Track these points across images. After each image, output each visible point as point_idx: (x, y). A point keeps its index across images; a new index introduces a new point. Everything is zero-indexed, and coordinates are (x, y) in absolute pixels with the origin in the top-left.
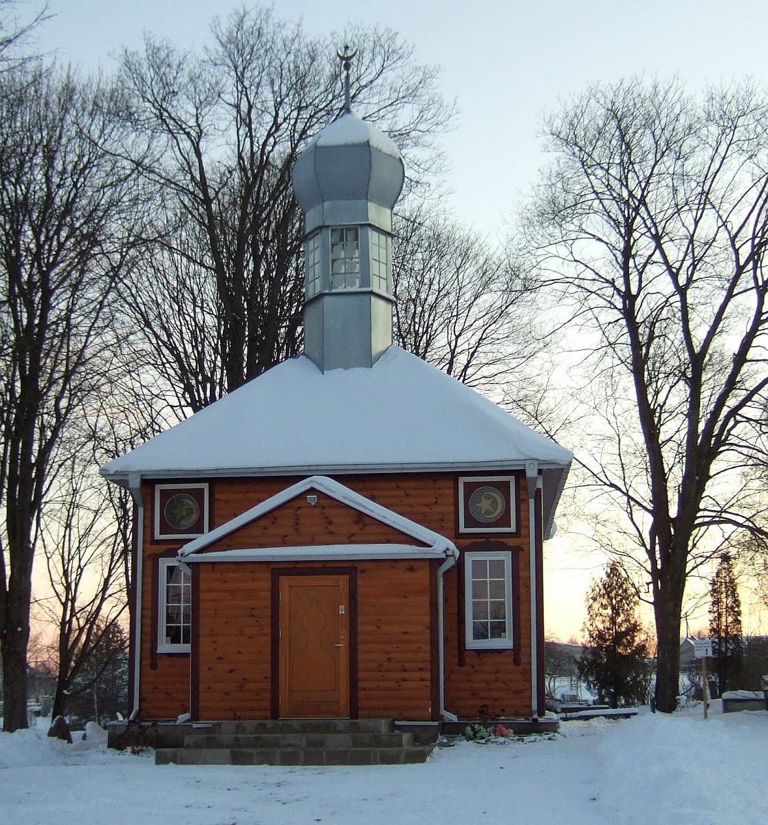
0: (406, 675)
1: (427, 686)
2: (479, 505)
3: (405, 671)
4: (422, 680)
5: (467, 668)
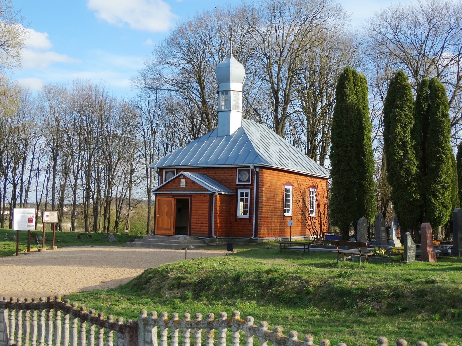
0: (202, 225)
5: (237, 223)
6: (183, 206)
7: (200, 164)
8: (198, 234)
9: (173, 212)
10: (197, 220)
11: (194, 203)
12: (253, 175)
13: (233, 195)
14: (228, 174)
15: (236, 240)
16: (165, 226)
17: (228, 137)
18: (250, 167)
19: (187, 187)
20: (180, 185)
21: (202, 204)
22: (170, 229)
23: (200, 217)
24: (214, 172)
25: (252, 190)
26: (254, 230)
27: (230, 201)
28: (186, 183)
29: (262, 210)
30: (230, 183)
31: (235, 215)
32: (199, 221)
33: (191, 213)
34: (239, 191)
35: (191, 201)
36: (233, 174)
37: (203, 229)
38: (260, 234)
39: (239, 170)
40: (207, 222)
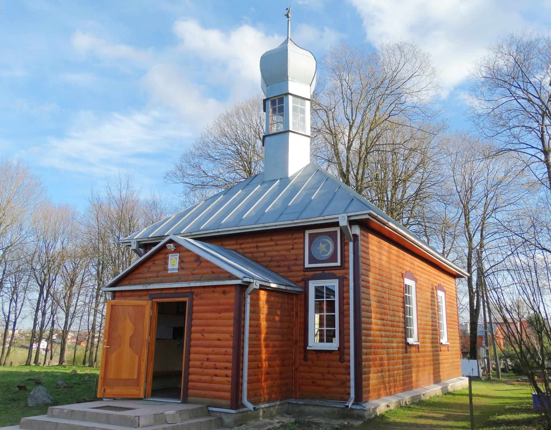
0: (217, 372)
1: (229, 381)
2: (318, 248)
3: (216, 368)
4: (227, 376)
5: (309, 363)
6: (172, 315)
7: (227, 225)
8: (205, 396)
9: (147, 337)
10: (205, 357)
11: (198, 312)
12: (344, 244)
13: (297, 294)
14: (283, 247)
15: (307, 409)
16: (125, 375)
17: (285, 180)
18: (336, 224)
19: (183, 272)
20: (166, 269)
21: (216, 315)
22: (137, 383)
23: (210, 350)
24: (254, 245)
25: (343, 281)
26: (352, 383)
27: (290, 305)
28: (181, 261)
29: (370, 329)
30: (289, 267)
31: (303, 344)
32: (208, 360)
33: (190, 339)
34: (312, 285)
35: (192, 306)
36: (296, 246)
37: (220, 383)
38: (369, 392)
39: (310, 235)
40: (230, 365)
